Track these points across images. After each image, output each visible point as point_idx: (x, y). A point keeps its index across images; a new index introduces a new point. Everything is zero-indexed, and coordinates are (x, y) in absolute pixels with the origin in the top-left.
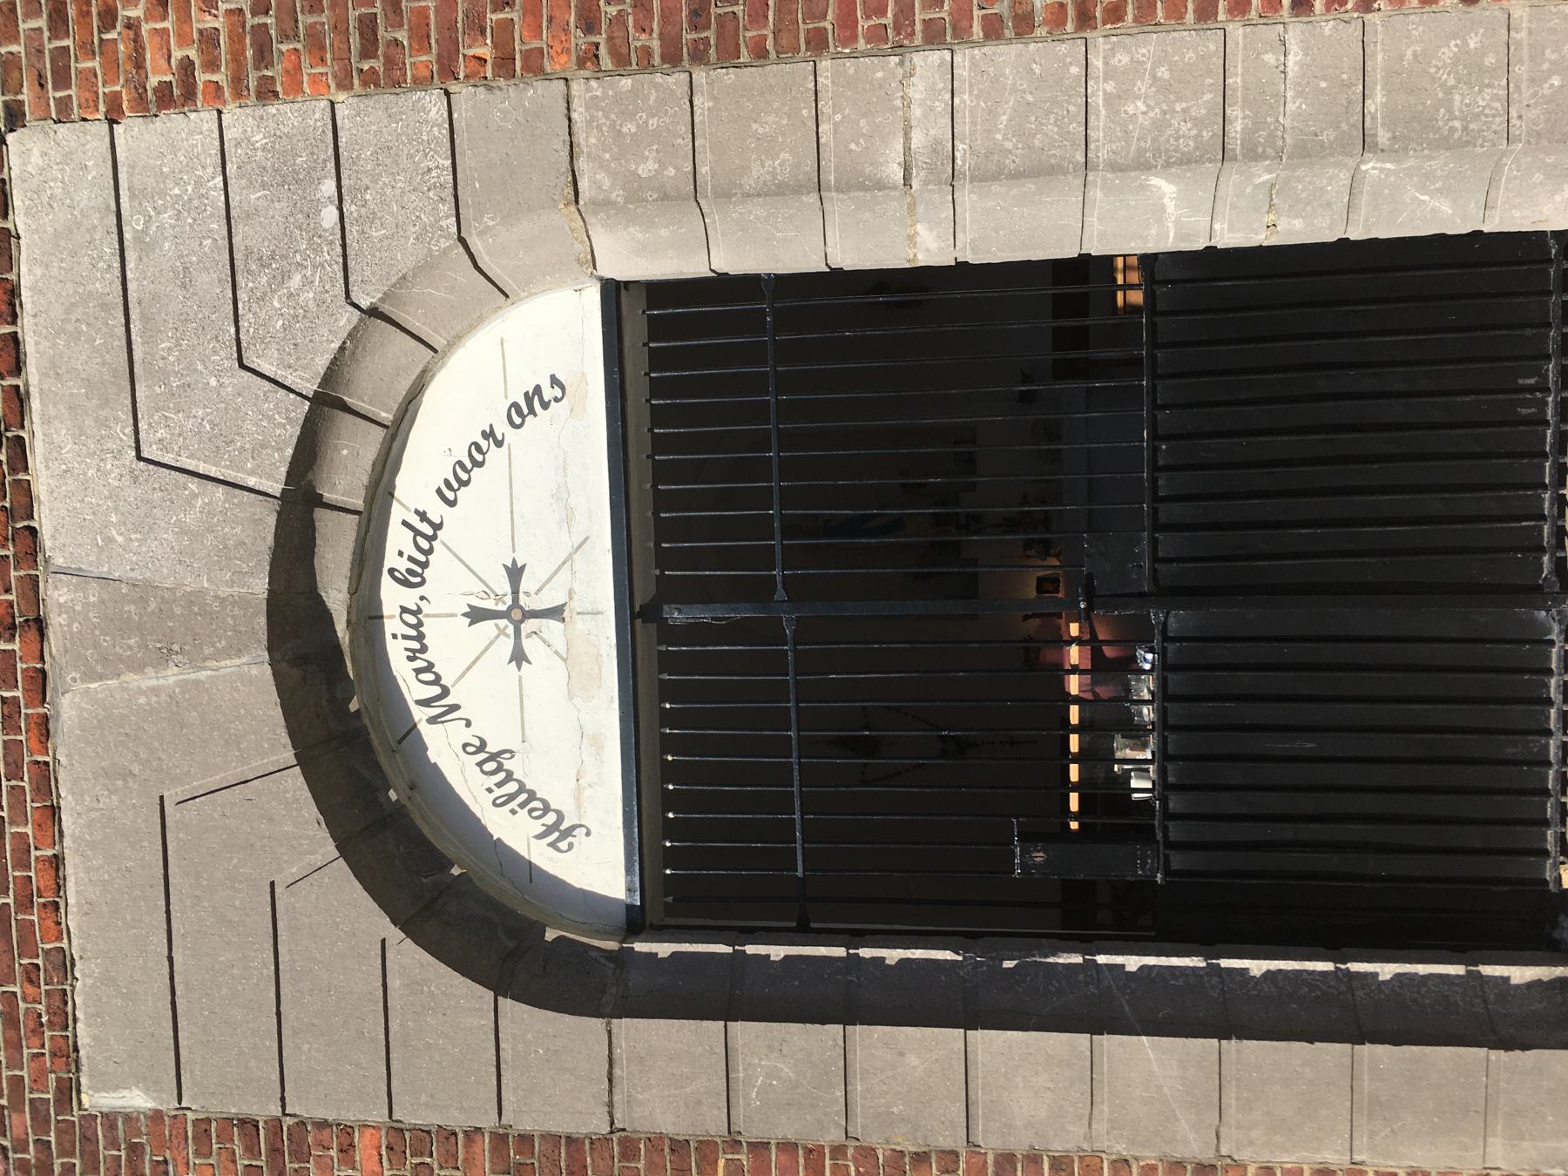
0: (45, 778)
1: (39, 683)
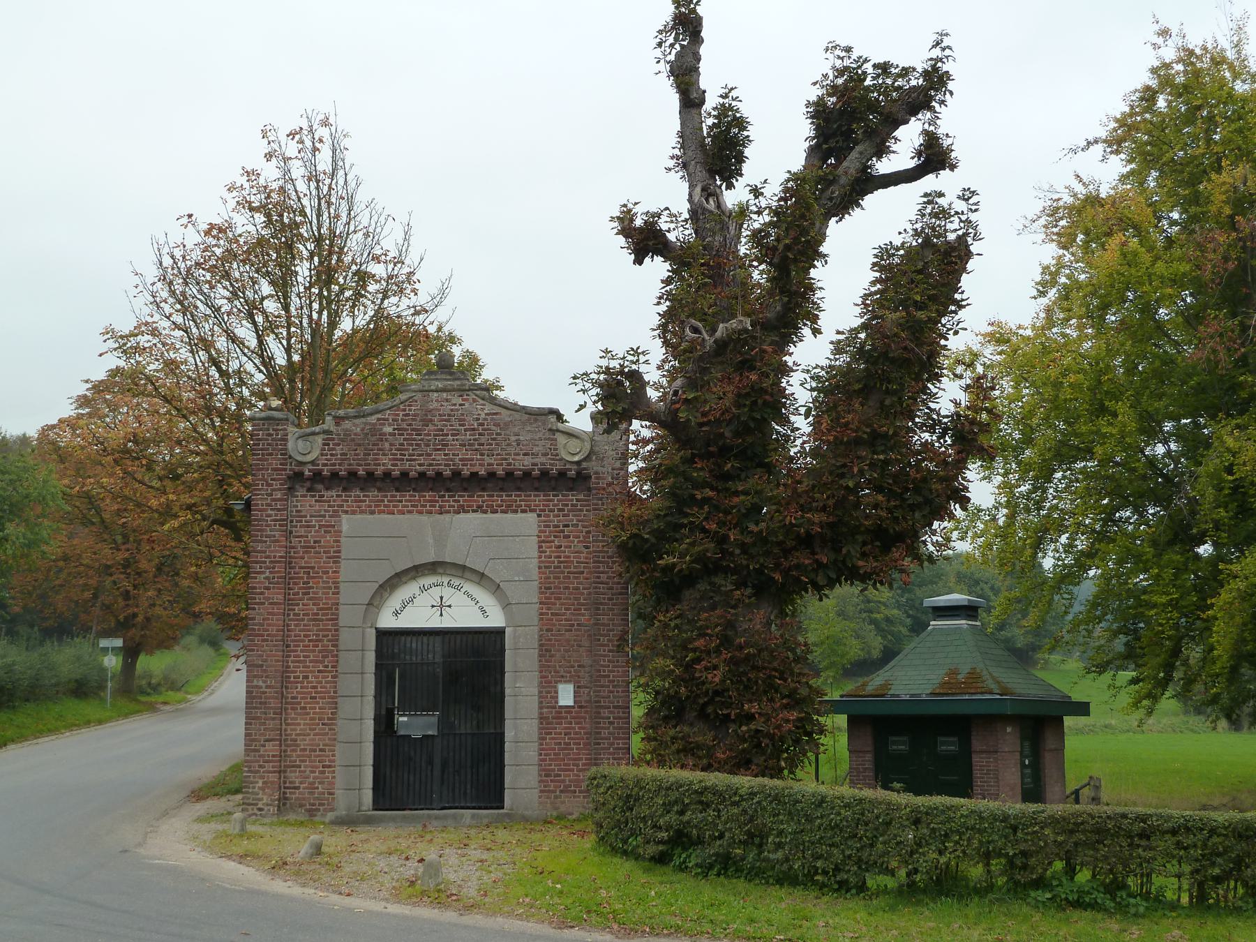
0: (410, 512)
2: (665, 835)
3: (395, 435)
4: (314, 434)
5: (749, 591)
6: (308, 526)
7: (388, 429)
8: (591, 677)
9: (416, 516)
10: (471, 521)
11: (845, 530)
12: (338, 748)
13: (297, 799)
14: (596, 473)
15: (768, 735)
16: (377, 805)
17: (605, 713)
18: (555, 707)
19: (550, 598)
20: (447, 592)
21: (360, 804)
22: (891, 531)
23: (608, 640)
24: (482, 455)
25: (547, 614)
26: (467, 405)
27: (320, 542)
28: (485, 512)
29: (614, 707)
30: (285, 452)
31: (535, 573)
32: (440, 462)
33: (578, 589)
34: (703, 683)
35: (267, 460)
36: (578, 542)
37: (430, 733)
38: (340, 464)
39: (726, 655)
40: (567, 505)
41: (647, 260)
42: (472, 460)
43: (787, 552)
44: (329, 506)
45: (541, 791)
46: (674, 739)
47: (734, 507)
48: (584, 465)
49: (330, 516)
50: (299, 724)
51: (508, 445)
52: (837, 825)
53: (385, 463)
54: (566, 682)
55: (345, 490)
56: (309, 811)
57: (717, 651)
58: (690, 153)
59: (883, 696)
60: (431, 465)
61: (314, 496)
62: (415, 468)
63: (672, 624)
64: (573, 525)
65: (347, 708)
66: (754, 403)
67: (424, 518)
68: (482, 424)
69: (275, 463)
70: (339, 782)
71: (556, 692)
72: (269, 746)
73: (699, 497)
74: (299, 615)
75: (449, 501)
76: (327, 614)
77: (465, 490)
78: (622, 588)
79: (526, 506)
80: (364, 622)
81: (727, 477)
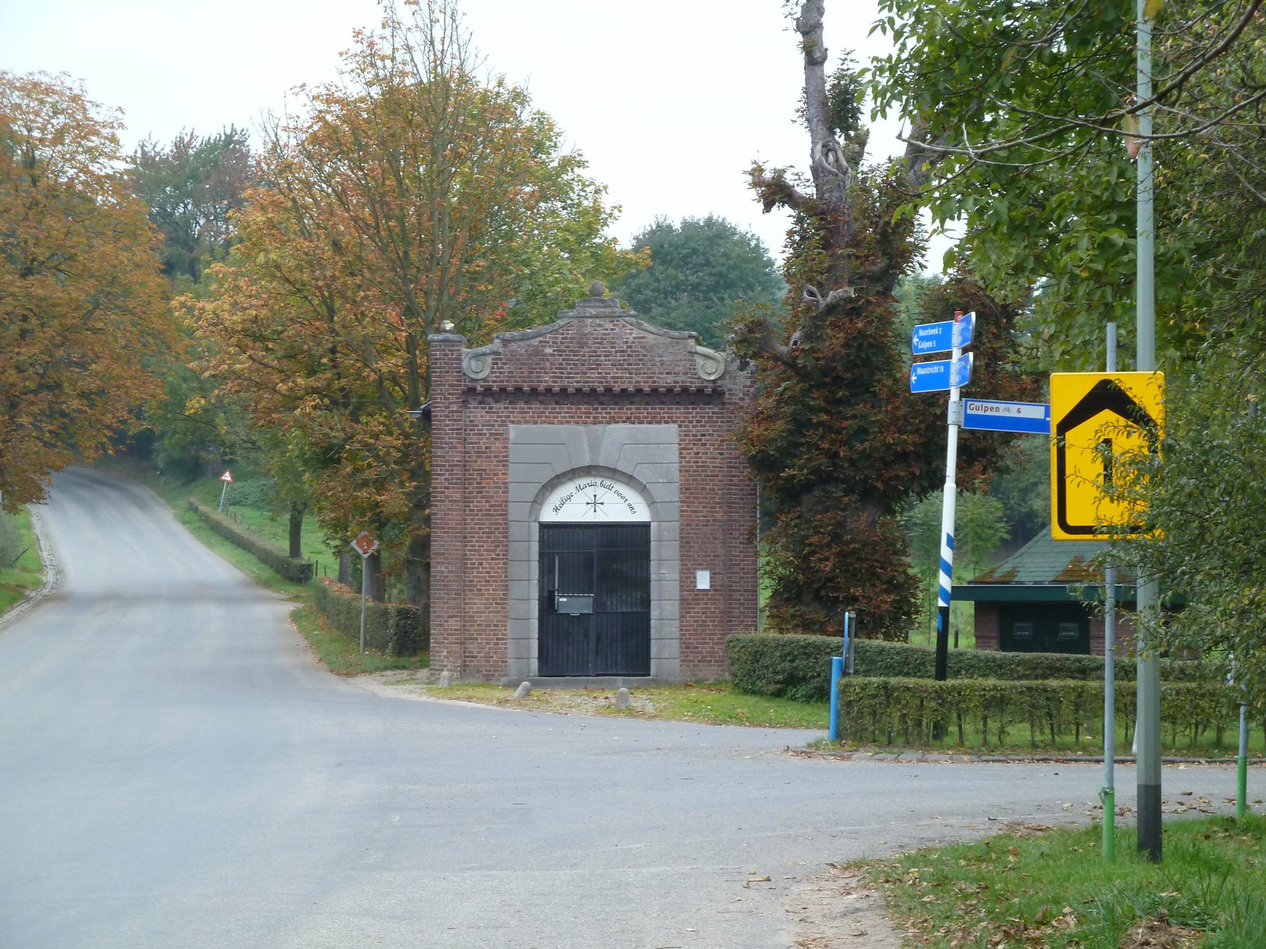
0: (568, 422)
1: (585, 423)
2: (780, 677)
3: (554, 355)
4: (484, 354)
5: (855, 497)
6: (480, 434)
7: (549, 351)
8: (725, 564)
9: (572, 426)
10: (620, 431)
11: (934, 448)
12: (510, 623)
13: (475, 666)
14: (730, 390)
15: (869, 614)
16: (542, 672)
17: (736, 595)
18: (693, 591)
19: (689, 498)
20: (600, 491)
21: (529, 671)
22: (974, 448)
23: (740, 534)
24: (631, 373)
25: (687, 511)
26: (617, 330)
27: (490, 448)
28: (633, 423)
29: (745, 591)
30: (459, 370)
31: (676, 476)
32: (594, 379)
33: (713, 490)
34: (817, 571)
35: (444, 377)
36: (714, 449)
37: (585, 612)
38: (507, 381)
39: (835, 549)
40: (704, 417)
41: (774, 209)
42: (622, 378)
43: (888, 465)
44: (498, 417)
45: (682, 661)
46: (793, 616)
47: (845, 428)
48: (719, 383)
49: (499, 426)
50: (476, 604)
51: (654, 365)
52: (891, 666)
53: (547, 380)
54: (703, 569)
55: (511, 403)
56: (486, 676)
57: (828, 546)
58: (813, 110)
59: (1008, 582)
60: (587, 382)
61: (484, 408)
62: (572, 385)
63: (793, 524)
64: (709, 435)
65: (516, 590)
66: (861, 345)
67: (581, 428)
68: (631, 347)
69: (452, 380)
70: (511, 652)
71: (695, 578)
72: (452, 621)
73: (815, 421)
74: (473, 510)
75: (602, 413)
76: (498, 510)
77: (616, 403)
78: (751, 490)
79: (668, 417)
80: (530, 516)
81: (839, 402)
